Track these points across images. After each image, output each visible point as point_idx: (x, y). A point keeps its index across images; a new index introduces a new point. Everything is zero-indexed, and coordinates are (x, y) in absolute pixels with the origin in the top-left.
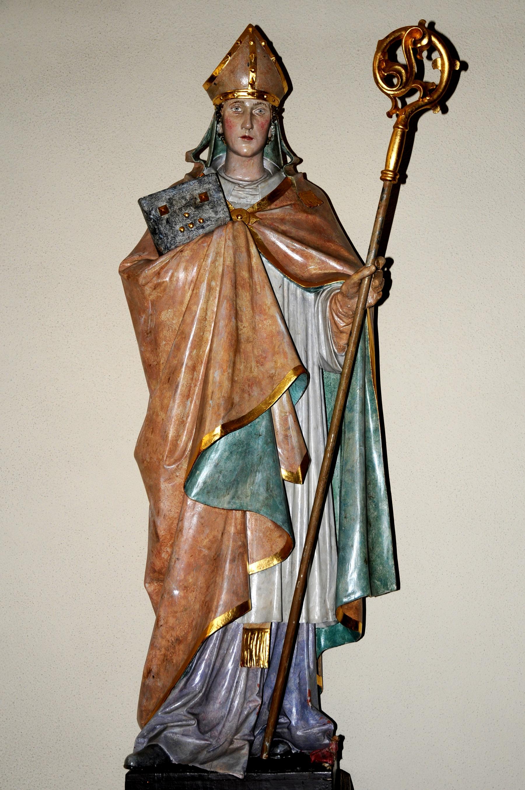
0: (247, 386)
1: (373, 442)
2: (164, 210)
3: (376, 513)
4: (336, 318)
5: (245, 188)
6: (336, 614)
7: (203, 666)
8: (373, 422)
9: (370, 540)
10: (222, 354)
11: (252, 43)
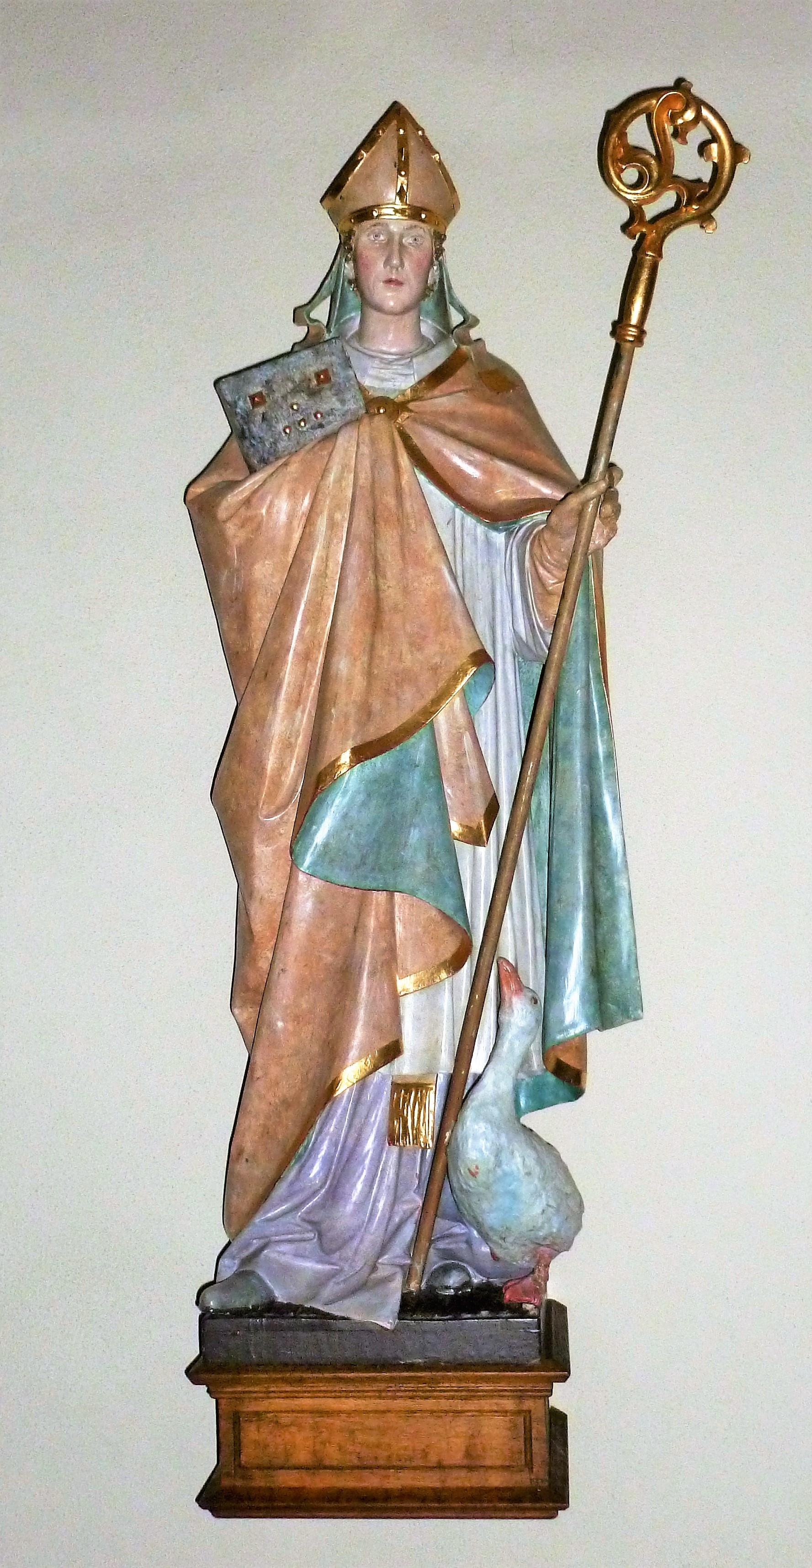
0: (393, 684)
1: (603, 777)
2: (257, 400)
3: (609, 894)
4: (541, 570)
5: (389, 363)
6: (545, 1059)
7: (326, 1143)
8: (603, 744)
9: (600, 938)
10: (351, 633)
11: (402, 132)
